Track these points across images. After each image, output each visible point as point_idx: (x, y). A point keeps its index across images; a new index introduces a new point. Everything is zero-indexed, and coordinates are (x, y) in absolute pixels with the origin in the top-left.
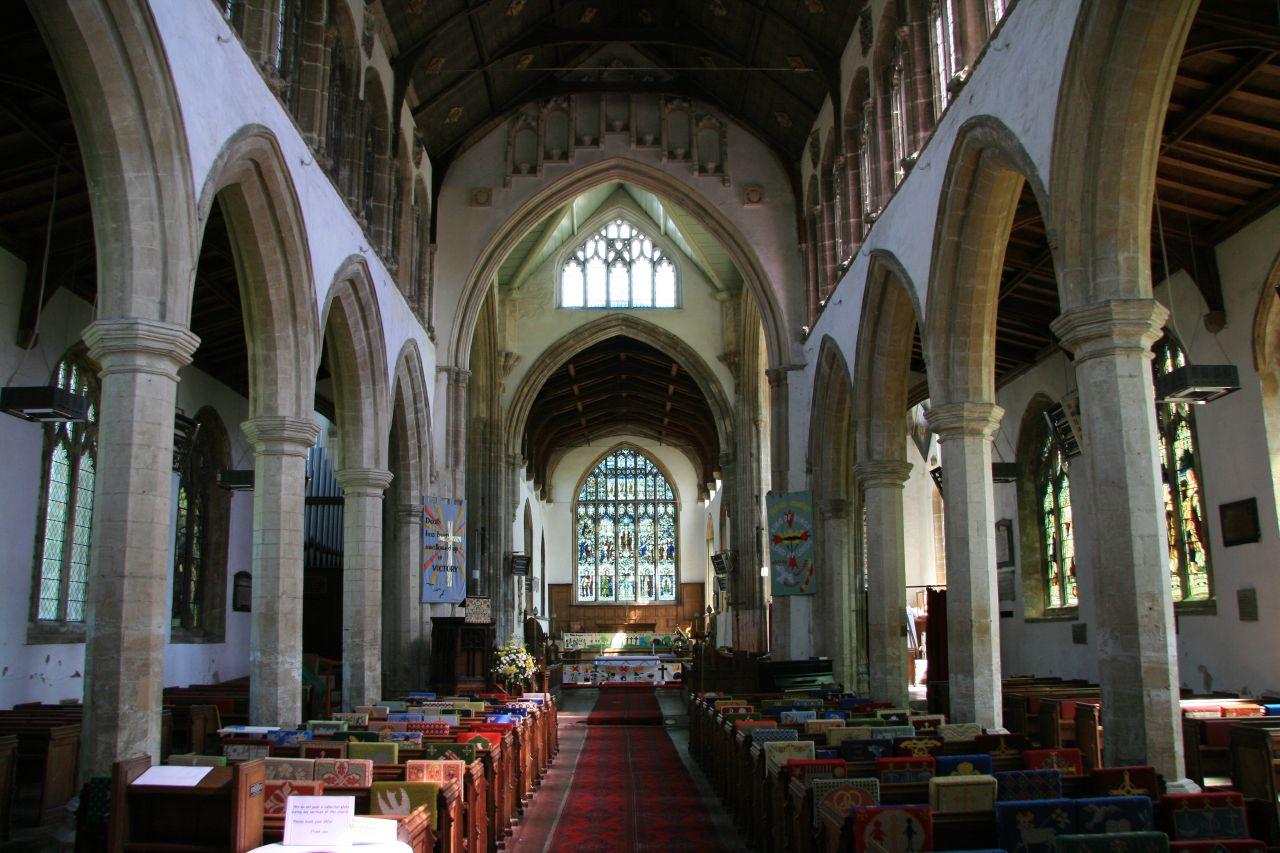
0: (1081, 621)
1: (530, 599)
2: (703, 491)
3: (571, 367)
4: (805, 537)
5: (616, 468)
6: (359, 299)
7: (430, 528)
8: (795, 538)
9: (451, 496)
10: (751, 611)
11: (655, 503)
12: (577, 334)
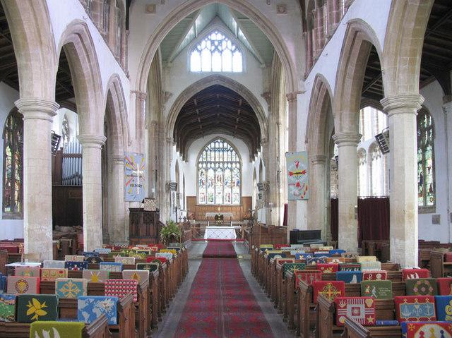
0: (437, 214)
1: (178, 202)
2: (252, 158)
3: (195, 101)
4: (304, 172)
5: (215, 148)
6: (84, 45)
7: (129, 167)
8: (299, 173)
9: (138, 152)
10: (43, 280)
11: (231, 163)
12: (198, 84)
